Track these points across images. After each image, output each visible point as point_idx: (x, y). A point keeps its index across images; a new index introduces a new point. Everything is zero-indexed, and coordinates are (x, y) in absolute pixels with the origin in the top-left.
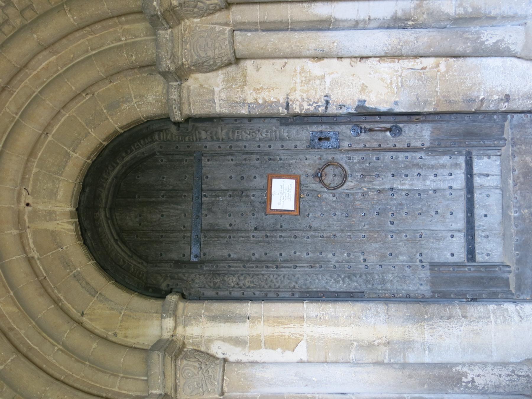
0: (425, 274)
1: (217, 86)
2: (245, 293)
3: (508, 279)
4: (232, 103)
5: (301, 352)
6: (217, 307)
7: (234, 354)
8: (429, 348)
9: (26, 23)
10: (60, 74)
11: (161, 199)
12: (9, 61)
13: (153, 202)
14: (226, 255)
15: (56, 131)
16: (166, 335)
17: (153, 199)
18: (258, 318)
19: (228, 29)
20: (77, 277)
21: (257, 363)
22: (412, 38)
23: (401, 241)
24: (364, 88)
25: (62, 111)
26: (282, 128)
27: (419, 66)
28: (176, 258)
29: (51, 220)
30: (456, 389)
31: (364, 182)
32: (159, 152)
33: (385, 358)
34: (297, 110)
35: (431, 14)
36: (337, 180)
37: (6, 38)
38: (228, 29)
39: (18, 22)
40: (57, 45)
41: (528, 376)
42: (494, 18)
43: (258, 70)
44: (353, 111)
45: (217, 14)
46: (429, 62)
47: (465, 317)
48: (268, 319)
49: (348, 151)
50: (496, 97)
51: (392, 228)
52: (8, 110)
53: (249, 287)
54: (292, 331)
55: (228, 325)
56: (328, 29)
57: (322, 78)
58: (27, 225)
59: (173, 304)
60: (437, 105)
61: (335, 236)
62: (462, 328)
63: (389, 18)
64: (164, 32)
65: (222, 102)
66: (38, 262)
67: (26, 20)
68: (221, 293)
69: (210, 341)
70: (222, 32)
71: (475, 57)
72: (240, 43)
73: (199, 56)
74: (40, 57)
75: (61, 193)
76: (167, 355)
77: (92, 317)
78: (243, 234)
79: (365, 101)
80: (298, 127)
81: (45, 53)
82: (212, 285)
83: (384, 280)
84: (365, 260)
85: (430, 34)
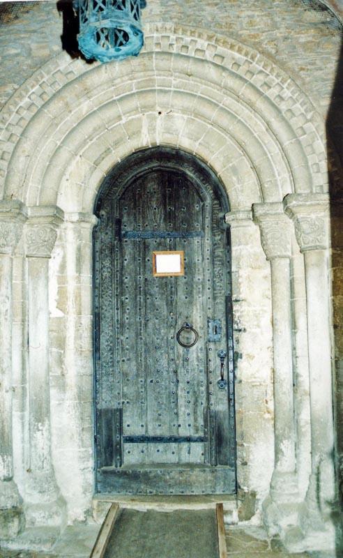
0: (114, 405)
1: (252, 247)
2: (98, 272)
3: (111, 465)
4: (238, 259)
5: (57, 313)
7: (54, 264)
9: (283, 112)
10: (253, 134)
11: (168, 207)
13: (166, 201)
14: (126, 257)
16: (66, 217)
17: (167, 202)
18: (80, 281)
20: (108, 151)
21: (48, 282)
23: (138, 388)
24: (251, 357)
26: (224, 298)
28: (123, 220)
29: (149, 130)
30: (33, 419)
31: (183, 361)
32: (204, 204)
33: (53, 373)
34: (234, 309)
35: (301, 402)
36: (183, 341)
38: (290, 254)
41: (43, 468)
46: (271, 406)
47: (83, 429)
48: (79, 288)
49: (206, 348)
50: (245, 455)
51: (149, 380)
53: (102, 275)
55: (75, 260)
57: (258, 326)
58: (145, 114)
61: (141, 339)
62: (75, 427)
65: (239, 251)
66: (118, 123)
68: (97, 254)
69: (63, 247)
77: (80, 164)
78: (142, 270)
79: (241, 358)
80: (224, 310)
82: (104, 248)
83: (109, 375)
84: (123, 361)
85: (288, 403)
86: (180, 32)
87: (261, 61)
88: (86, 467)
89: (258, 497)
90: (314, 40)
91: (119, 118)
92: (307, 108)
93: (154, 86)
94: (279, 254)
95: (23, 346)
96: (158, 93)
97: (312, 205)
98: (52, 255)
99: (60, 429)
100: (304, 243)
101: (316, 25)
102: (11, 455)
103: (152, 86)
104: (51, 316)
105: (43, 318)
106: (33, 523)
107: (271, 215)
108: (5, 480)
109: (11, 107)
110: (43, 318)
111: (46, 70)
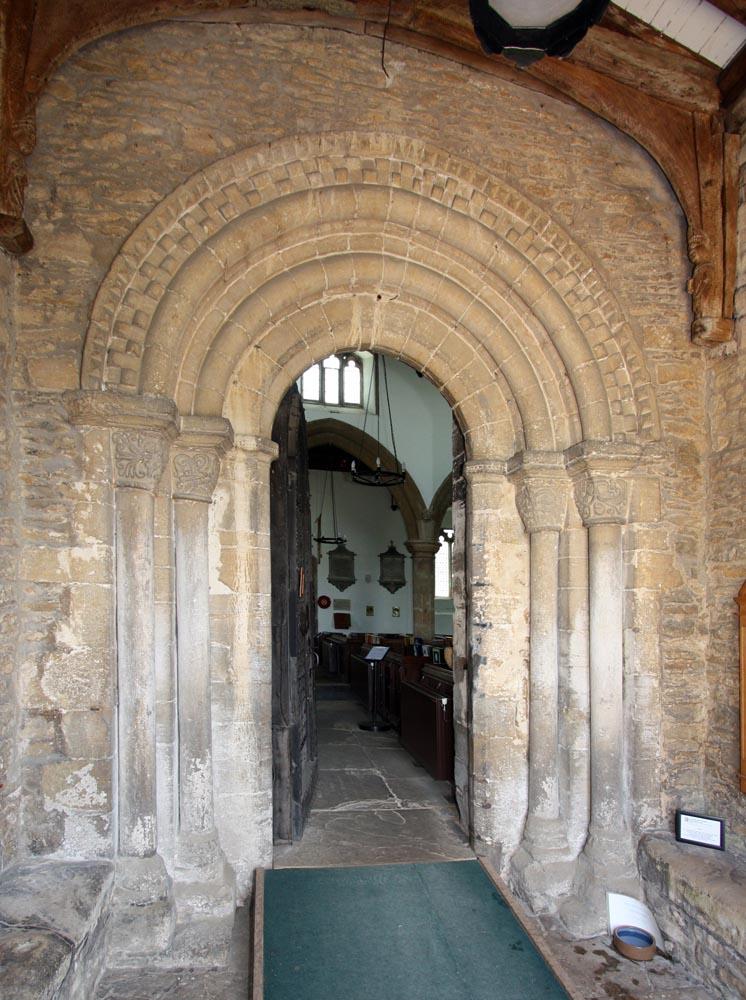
4: (484, 527)
5: (221, 589)
6: (265, 498)
7: (215, 515)
8: (226, 726)
10: (520, 348)
12: (539, 297)
15: (458, 338)
16: (237, 440)
19: (562, 526)
22: (549, 709)
24: (498, 663)
25: (480, 345)
27: (519, 718)
29: (363, 321)
34: (475, 595)
37: (562, 296)
38: (562, 526)
39: (577, 311)
40: (552, 348)
41: (203, 827)
42: (568, 788)
43: (517, 556)
44: (473, 653)
45: (578, 516)
46: (524, 728)
47: (261, 764)
48: (254, 553)
52: (485, 287)
54: (243, 580)
56: (559, 627)
58: (358, 294)
59: (269, 449)
60: (480, 736)
63: (571, 686)
64: (562, 460)
65: (485, 516)
66: (316, 302)
67: (580, 320)
69: (229, 488)
70: (560, 521)
71: (529, 775)
72: (548, 538)
73: (536, 495)
74: (541, 329)
75: (391, 335)
76: (223, 439)
79: (485, 664)
81: (544, 334)
86: (434, 160)
87: (553, 233)
88: (265, 818)
89: (504, 850)
90: (626, 214)
91: (319, 294)
92: (613, 315)
93: (380, 249)
94: (549, 524)
95: (171, 639)
96: (386, 261)
97: (617, 459)
98: (213, 499)
99: (226, 762)
100: (596, 513)
101: (630, 191)
102: (155, 815)
103: (376, 248)
104: (212, 592)
105: (201, 600)
106: (188, 915)
107: (547, 469)
108: (145, 856)
109: (151, 232)
110: (201, 600)
111: (213, 177)
